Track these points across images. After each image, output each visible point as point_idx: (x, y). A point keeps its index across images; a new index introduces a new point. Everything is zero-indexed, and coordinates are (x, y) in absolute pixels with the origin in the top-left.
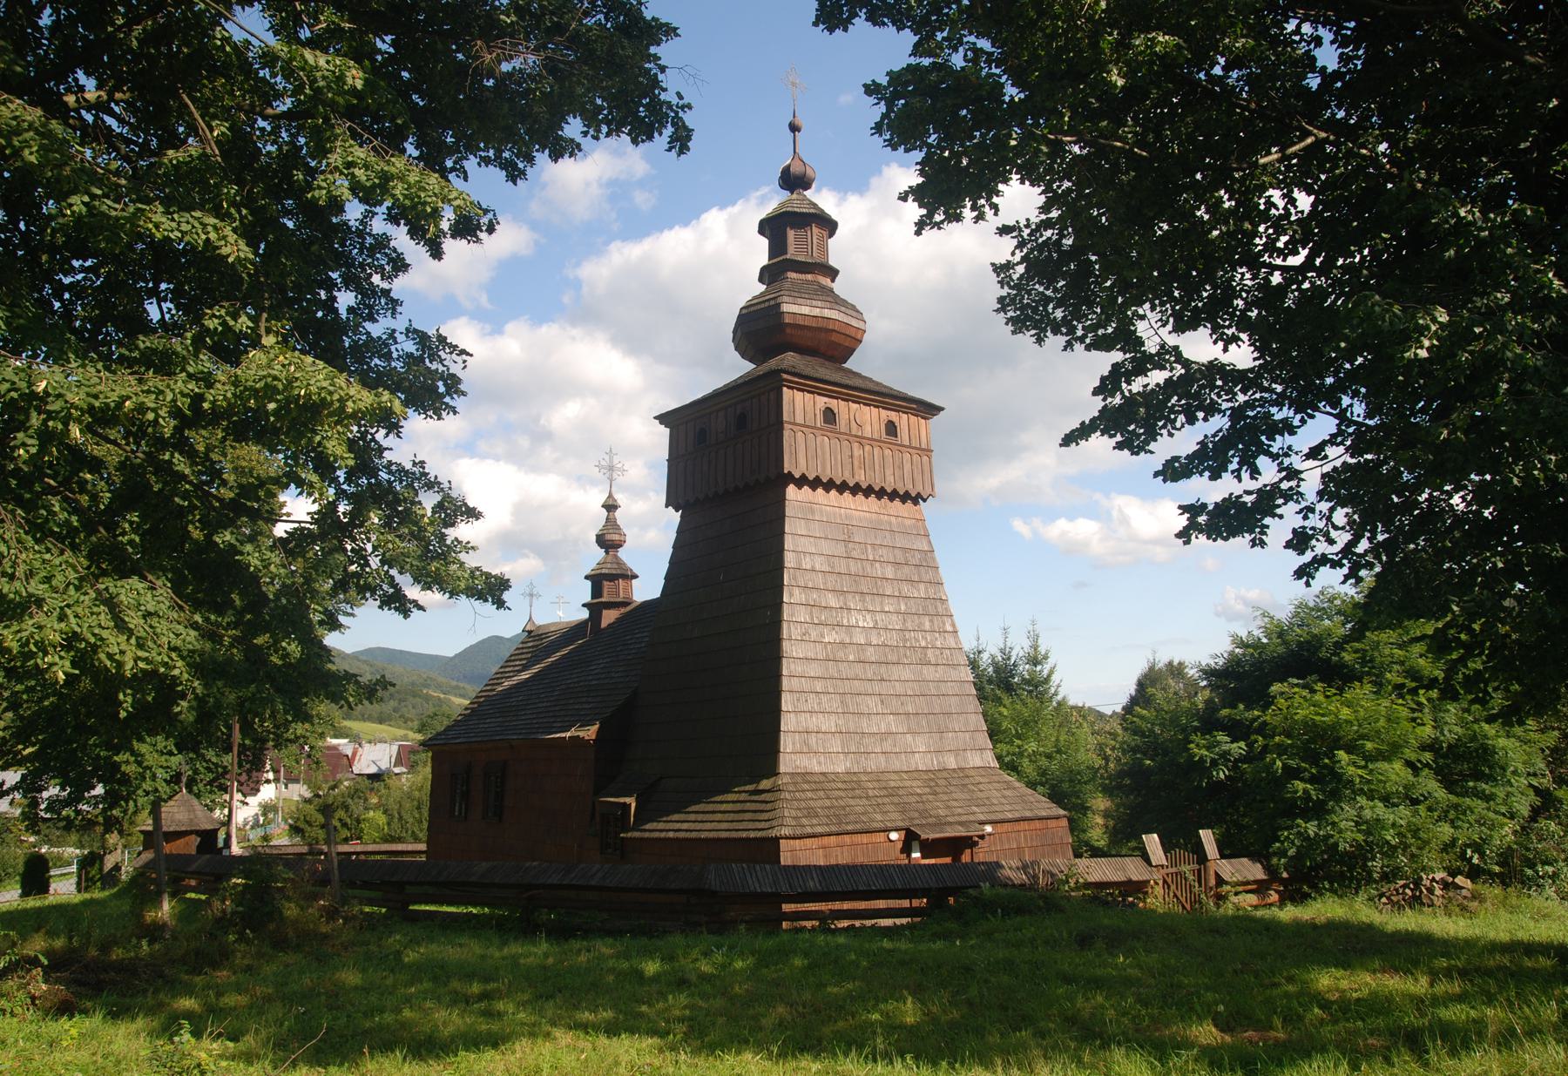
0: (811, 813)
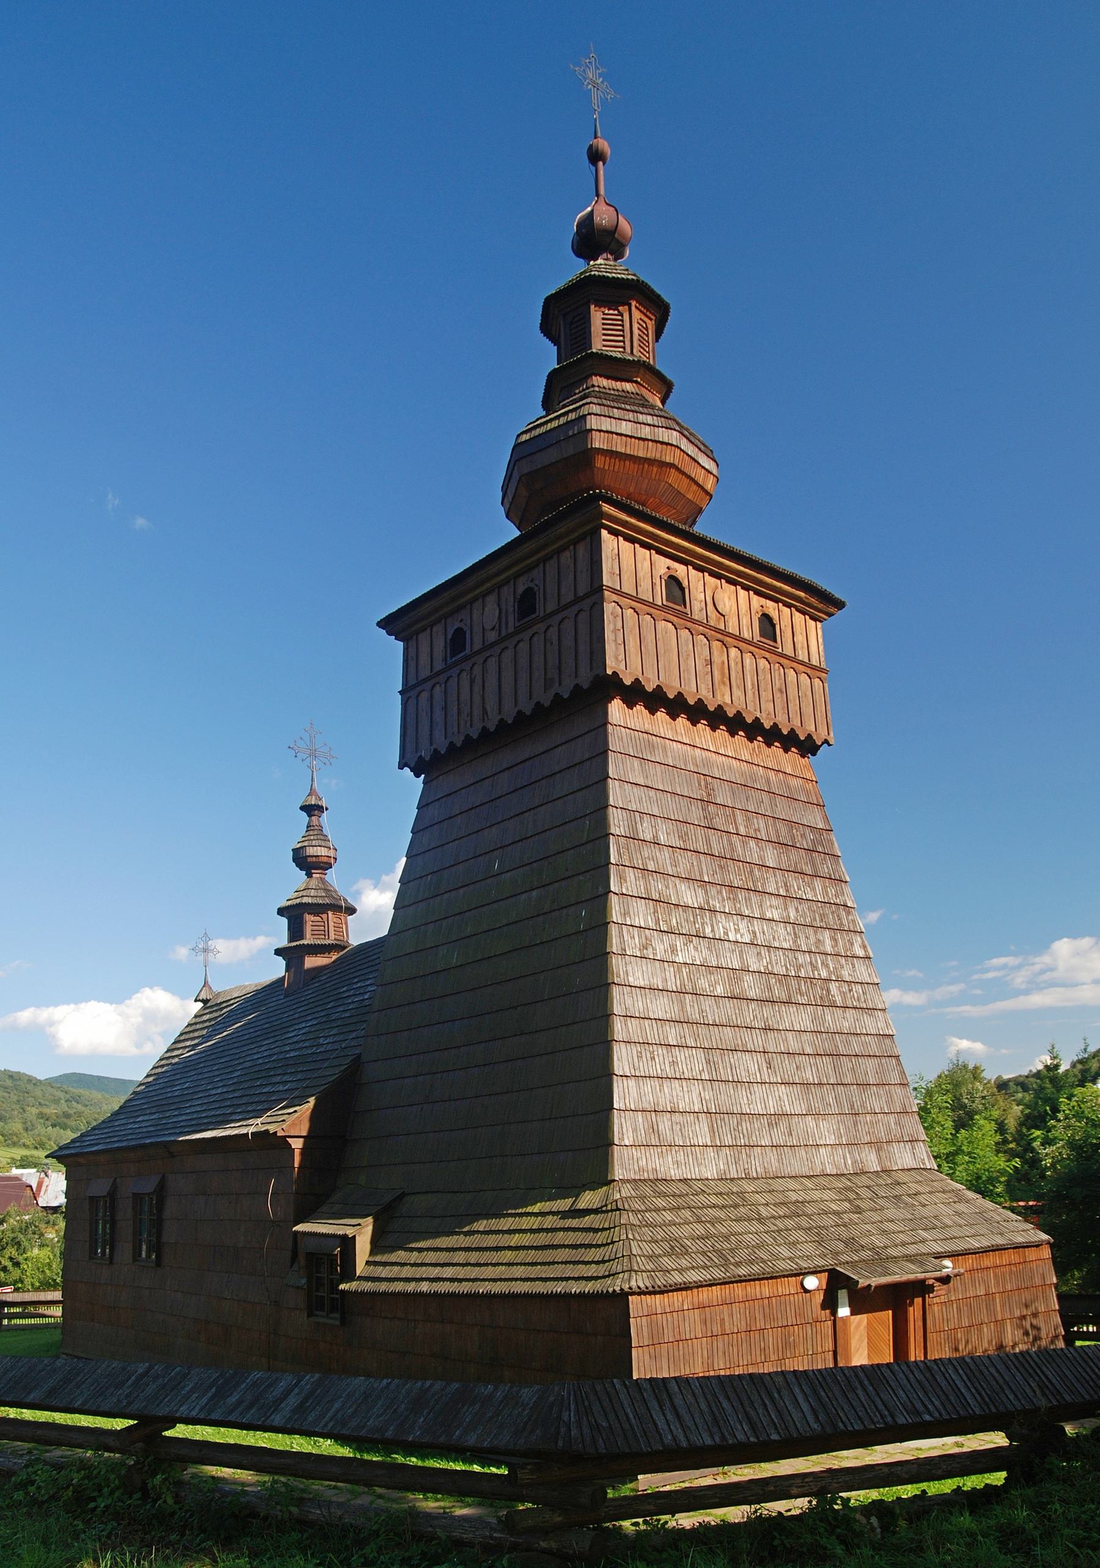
0: (677, 1249)
